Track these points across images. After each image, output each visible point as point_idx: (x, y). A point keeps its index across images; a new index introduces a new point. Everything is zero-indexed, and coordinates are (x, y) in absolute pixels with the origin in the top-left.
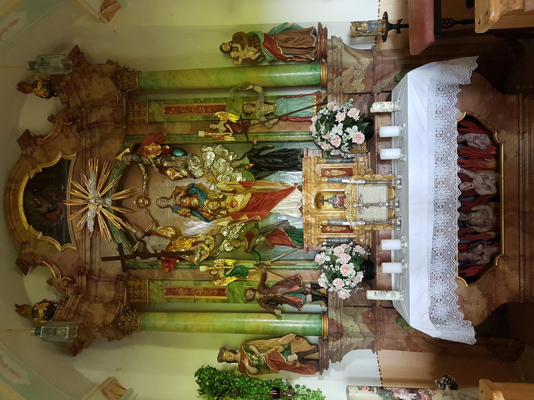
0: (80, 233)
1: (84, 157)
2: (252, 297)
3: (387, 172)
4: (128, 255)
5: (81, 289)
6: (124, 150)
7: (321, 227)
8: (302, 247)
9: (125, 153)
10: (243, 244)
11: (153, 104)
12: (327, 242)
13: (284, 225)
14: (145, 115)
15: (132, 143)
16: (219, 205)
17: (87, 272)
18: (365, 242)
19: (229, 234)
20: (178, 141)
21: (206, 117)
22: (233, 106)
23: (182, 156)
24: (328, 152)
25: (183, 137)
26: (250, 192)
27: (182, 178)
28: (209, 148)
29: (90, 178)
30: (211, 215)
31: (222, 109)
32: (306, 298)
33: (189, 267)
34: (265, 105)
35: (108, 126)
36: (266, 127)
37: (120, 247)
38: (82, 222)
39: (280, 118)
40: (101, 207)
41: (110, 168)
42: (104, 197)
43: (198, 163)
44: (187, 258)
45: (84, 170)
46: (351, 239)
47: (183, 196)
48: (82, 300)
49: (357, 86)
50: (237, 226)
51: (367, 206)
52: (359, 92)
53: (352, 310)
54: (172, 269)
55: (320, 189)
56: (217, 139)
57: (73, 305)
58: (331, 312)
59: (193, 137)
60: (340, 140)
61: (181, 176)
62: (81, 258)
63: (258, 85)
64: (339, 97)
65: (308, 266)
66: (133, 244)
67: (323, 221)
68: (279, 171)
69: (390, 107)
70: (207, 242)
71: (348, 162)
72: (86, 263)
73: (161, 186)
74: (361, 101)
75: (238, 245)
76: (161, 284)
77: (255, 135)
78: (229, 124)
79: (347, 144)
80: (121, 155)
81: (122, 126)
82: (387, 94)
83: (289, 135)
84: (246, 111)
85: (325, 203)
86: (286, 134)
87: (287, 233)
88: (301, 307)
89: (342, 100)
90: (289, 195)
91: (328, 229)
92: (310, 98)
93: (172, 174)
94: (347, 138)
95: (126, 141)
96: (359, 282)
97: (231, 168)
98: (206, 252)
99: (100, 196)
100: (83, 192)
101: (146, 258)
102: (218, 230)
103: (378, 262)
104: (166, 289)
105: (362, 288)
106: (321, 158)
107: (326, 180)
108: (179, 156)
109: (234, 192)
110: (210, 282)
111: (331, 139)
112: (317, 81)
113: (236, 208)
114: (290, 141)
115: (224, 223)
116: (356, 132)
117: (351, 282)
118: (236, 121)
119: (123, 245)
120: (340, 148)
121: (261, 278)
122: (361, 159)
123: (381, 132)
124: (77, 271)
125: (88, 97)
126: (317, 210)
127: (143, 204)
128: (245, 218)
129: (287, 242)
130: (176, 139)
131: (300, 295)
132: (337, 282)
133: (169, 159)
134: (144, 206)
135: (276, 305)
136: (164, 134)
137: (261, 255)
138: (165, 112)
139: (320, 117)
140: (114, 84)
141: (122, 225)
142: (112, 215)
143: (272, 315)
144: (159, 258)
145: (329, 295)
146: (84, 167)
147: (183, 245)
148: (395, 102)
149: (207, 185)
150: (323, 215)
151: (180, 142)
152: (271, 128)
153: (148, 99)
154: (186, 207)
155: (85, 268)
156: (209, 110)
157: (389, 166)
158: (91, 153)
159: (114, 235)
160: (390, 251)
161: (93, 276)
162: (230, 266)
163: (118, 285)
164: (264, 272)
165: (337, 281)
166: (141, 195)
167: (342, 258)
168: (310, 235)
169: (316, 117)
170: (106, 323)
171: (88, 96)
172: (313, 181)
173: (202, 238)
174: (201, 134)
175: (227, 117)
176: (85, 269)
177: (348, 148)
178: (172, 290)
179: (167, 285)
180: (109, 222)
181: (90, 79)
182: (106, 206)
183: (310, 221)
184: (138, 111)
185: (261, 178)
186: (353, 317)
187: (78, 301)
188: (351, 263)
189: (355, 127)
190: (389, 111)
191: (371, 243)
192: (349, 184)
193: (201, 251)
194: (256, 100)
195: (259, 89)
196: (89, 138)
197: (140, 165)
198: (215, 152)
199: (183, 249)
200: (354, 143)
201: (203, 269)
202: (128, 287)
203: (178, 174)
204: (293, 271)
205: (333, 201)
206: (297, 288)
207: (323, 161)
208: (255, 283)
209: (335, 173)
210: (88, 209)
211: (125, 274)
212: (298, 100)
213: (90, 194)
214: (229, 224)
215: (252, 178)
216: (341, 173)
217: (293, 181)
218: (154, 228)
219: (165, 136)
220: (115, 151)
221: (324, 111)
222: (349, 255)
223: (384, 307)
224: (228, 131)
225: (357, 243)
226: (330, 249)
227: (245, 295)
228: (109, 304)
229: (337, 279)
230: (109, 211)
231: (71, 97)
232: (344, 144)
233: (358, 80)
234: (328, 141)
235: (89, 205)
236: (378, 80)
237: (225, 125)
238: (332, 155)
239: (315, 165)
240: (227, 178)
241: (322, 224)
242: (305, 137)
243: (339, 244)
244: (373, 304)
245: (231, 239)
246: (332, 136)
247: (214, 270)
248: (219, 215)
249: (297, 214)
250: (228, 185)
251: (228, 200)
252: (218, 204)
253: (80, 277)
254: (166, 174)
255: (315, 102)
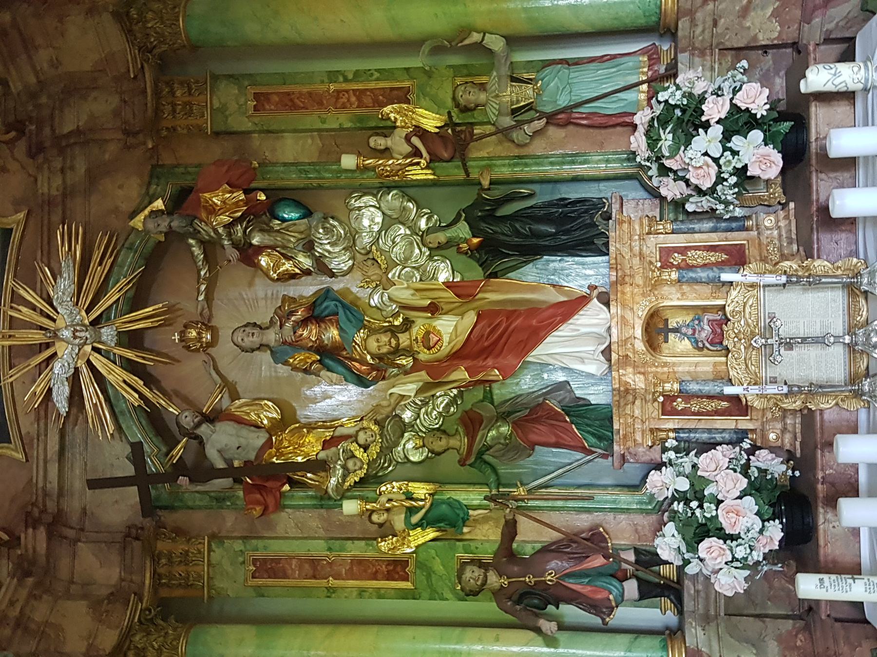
0: (32, 416)
1: (46, 222)
2: (479, 583)
3: (843, 253)
4: (158, 474)
5: (33, 562)
6: (150, 203)
7: (661, 399)
8: (608, 453)
9: (152, 212)
10: (454, 442)
11: (223, 85)
12: (676, 439)
13: (560, 395)
14: (203, 112)
15: (169, 186)
16: (394, 342)
17: (50, 519)
18: (782, 441)
19: (419, 416)
20: (288, 180)
21: (360, 119)
22: (428, 89)
23: (298, 219)
24: (679, 205)
25: (300, 171)
26: (474, 309)
27: (298, 274)
28: (368, 200)
29: (61, 276)
30: (373, 367)
31: (402, 96)
32: (623, 589)
33: (314, 502)
34: (512, 86)
35: (106, 141)
36: (513, 141)
37: (137, 453)
38: (39, 388)
39: (551, 118)
40: (88, 348)
41: (113, 249)
42: (98, 324)
43: (339, 237)
44: (310, 479)
45: (45, 253)
46: (742, 435)
47: (302, 321)
48: (35, 592)
49: (758, 25)
50: (438, 398)
51: (789, 344)
52: (763, 43)
53: (750, 625)
54: (271, 509)
55: (657, 300)
56: (388, 176)
57: (12, 603)
58: (693, 630)
59: (326, 171)
60: (713, 170)
61: (297, 271)
62: (34, 481)
63: (494, 31)
64: (708, 58)
65: (625, 502)
66: (172, 443)
67: (666, 385)
68: (545, 257)
69: (855, 76)
70: (362, 438)
71: (731, 230)
72: (46, 494)
73: (245, 296)
74: (766, 67)
75: (441, 446)
76: (242, 548)
77: (484, 163)
78: (420, 137)
79: (733, 180)
80: (141, 217)
81: (145, 143)
82: (842, 47)
83: (573, 163)
84: (462, 102)
85: (671, 336)
86: (565, 159)
87: (568, 415)
88: (609, 615)
89: (716, 66)
90: (576, 317)
91: (680, 405)
92: (631, 64)
93: (272, 265)
94: (733, 164)
95: (155, 180)
96: (771, 551)
97: (423, 249)
98: (359, 464)
99: (87, 322)
100: (41, 309)
101: (206, 480)
102: (393, 406)
103: (821, 495)
104: (255, 561)
105: (778, 567)
106: (658, 219)
107: (674, 275)
108: (291, 220)
109: (434, 309)
110: (370, 542)
111: (690, 168)
112: (650, 16)
113: (439, 350)
114: (576, 179)
115: (408, 388)
116: (758, 147)
117: (748, 551)
118: (437, 127)
119: (145, 446)
120: (712, 190)
121: (502, 534)
122: (768, 221)
123: (834, 142)
124: (24, 516)
125: (57, 68)
126: (649, 356)
127: (199, 342)
128: (461, 374)
129: (568, 440)
130: (282, 175)
131: (607, 581)
132: (710, 547)
133: (266, 228)
134: (201, 346)
135: (543, 606)
136: (251, 163)
137: (502, 470)
138: (255, 106)
139: (658, 112)
140: (122, 32)
141: (142, 396)
142: (118, 370)
143: (531, 634)
144: (237, 481)
145: (686, 582)
146: (46, 247)
147: (303, 445)
148: (869, 64)
149: (363, 294)
150: (666, 369)
151: (290, 184)
152: (526, 145)
153: (210, 72)
154: (310, 349)
155: (45, 505)
156: (367, 100)
157: (851, 236)
158: (64, 212)
159: (121, 421)
160: (855, 467)
161: (63, 529)
162: (422, 500)
163: (128, 551)
164: (511, 517)
165: (709, 545)
166: (195, 319)
167: (721, 483)
168: (630, 420)
169: (648, 111)
170: (95, 654)
171: (55, 64)
172: (639, 280)
173: (349, 428)
174: (349, 161)
175: (413, 119)
176: (44, 511)
177: (736, 190)
178: (268, 563)
179: (257, 550)
180: (109, 387)
181: (61, 21)
182: (100, 346)
183: (632, 383)
184: (185, 104)
185: (499, 274)
186: (753, 645)
187: (23, 593)
188: (749, 497)
189: (757, 135)
190: (852, 87)
191: (798, 444)
192: (737, 286)
193: (346, 460)
194: (488, 73)
195: (496, 43)
196: (59, 173)
197: (191, 241)
198: (384, 209)
199: (299, 456)
200: (752, 177)
201: (350, 507)
202: (155, 559)
203: (287, 266)
204: (584, 516)
205: (694, 330)
206: (598, 561)
207: (664, 228)
208: (487, 545)
209: (697, 257)
210: (55, 354)
211: (148, 522)
212: (598, 70)
213: (60, 315)
214: (419, 392)
215: (476, 273)
216: (713, 257)
217: (583, 282)
218: (226, 403)
219: (255, 169)
220: (126, 207)
221: (670, 95)
222: (740, 476)
223: (837, 620)
224: (417, 153)
225: (759, 444)
226: (686, 459)
227: (459, 577)
228: (103, 601)
229: (711, 539)
230: (110, 360)
231: (11, 68)
232: (726, 180)
233: (762, 9)
234: (680, 174)
235: (58, 344)
236: (815, 8)
237: (408, 139)
238: (690, 210)
239: (641, 239)
240: (414, 275)
241: (664, 391)
242: (616, 168)
243: (711, 446)
244: (811, 607)
245: (424, 430)
246: (692, 159)
247: (380, 510)
248: (391, 370)
249: (595, 367)
250: (417, 290)
251: (417, 330)
252: (392, 340)
253: (30, 530)
254: (257, 266)
255: (643, 73)
